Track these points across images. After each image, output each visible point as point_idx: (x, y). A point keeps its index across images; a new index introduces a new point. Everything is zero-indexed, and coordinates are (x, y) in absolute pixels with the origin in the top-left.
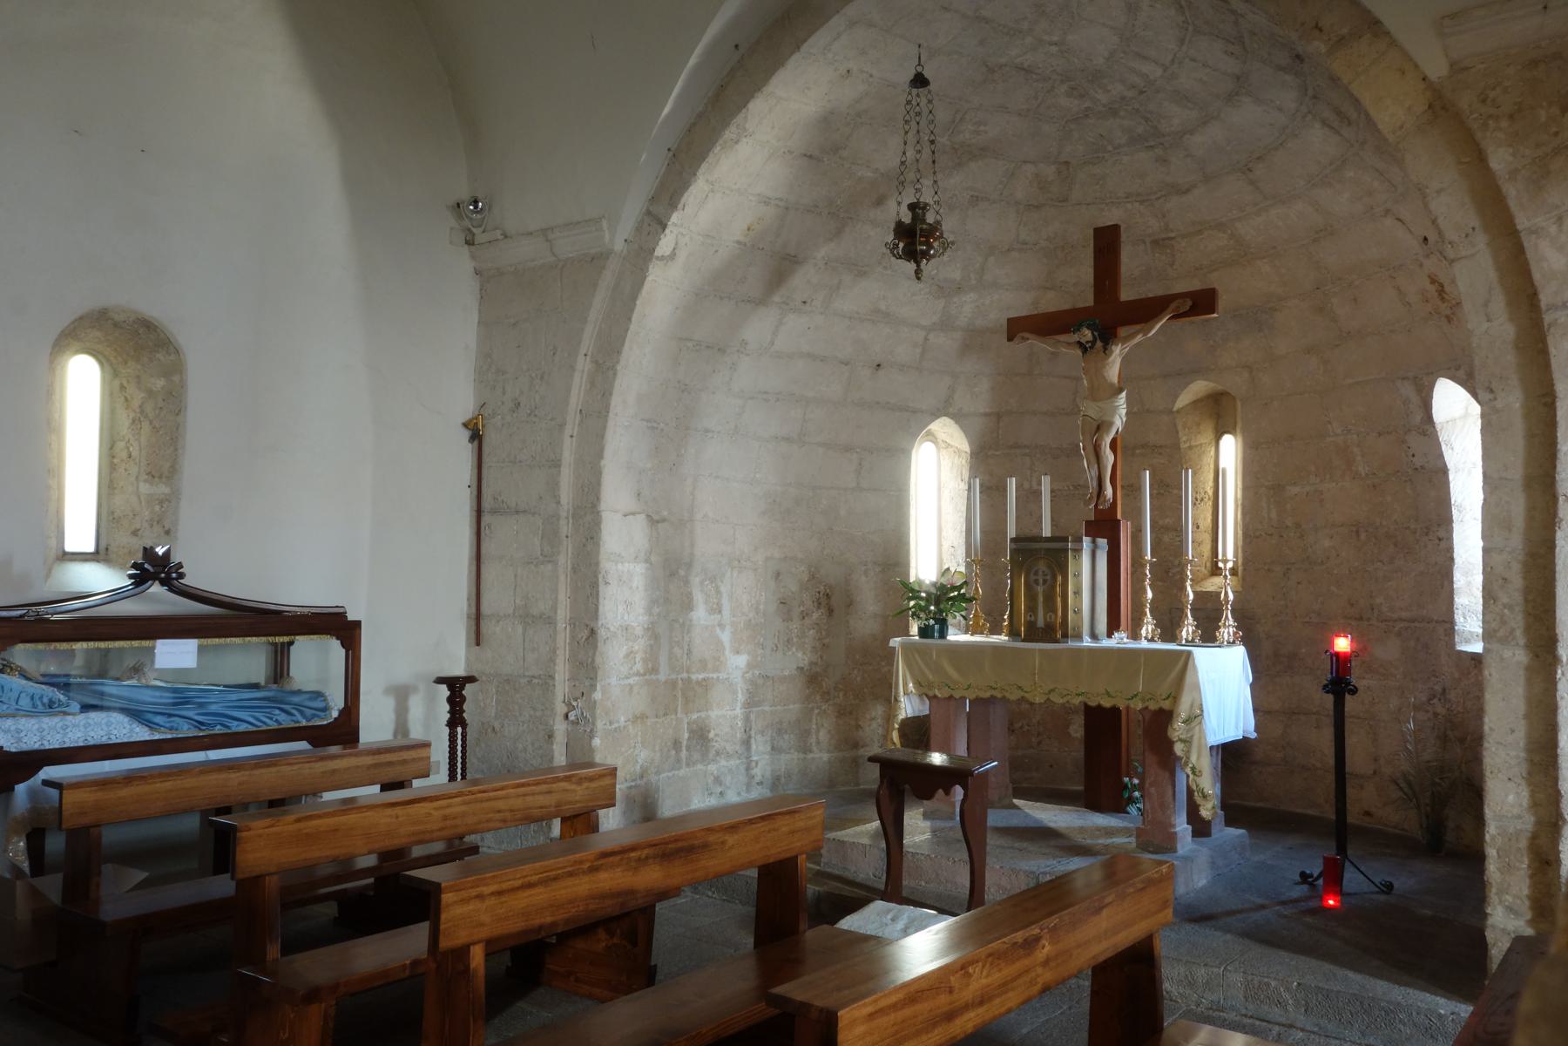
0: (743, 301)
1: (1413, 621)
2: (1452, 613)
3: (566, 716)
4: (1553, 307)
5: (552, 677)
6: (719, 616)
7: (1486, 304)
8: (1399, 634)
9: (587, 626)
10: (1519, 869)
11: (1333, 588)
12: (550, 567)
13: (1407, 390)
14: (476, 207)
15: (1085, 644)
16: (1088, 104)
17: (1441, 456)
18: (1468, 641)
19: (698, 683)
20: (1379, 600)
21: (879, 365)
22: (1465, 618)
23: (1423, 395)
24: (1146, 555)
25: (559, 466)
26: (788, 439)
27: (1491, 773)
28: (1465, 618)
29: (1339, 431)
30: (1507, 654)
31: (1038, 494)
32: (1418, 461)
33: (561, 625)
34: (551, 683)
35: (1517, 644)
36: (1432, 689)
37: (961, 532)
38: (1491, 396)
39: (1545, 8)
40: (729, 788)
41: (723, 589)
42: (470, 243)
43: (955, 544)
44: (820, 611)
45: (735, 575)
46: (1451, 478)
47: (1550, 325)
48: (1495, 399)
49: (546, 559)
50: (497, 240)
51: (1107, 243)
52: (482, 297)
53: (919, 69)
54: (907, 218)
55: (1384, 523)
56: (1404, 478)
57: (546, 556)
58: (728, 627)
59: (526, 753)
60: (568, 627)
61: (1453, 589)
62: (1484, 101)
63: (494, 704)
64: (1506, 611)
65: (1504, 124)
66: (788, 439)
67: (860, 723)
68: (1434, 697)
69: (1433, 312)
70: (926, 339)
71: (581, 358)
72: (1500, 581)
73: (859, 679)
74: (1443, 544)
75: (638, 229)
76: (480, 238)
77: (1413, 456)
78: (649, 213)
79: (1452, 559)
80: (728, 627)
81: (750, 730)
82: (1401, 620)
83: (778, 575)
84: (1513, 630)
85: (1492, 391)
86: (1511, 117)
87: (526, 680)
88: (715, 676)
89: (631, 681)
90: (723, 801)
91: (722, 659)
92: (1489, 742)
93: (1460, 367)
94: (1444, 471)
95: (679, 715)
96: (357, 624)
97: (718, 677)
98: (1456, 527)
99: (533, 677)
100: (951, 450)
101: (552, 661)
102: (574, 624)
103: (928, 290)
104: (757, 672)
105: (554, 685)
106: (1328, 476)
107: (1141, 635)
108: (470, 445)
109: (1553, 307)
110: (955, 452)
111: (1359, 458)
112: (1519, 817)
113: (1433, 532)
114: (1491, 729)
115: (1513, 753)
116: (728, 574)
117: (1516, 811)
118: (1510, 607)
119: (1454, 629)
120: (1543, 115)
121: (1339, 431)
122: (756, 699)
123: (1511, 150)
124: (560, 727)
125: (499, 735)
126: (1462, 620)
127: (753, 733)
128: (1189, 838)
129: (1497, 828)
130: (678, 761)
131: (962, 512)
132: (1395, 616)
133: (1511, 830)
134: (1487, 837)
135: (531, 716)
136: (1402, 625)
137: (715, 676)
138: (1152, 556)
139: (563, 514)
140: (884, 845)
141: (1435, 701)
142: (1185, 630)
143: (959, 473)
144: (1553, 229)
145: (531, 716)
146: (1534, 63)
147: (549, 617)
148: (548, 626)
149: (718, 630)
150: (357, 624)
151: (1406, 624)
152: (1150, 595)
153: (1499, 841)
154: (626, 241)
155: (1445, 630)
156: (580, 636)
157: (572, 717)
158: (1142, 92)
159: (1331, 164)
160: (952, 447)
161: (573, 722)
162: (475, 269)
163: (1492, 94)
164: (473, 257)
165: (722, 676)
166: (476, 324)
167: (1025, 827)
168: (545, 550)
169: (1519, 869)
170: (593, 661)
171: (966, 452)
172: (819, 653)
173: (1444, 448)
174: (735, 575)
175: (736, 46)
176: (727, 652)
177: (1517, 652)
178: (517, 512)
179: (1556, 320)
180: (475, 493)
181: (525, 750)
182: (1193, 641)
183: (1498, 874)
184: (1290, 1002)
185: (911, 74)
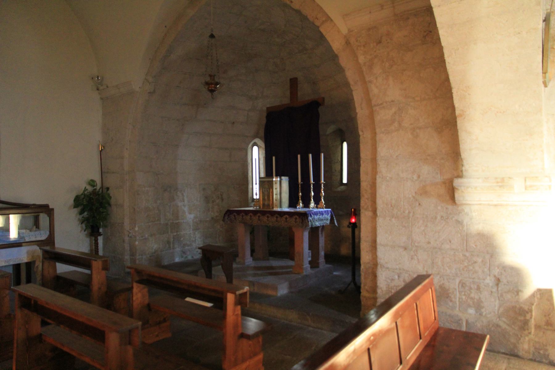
3: (129, 236)
4: (375, 106)
6: (183, 203)
14: (98, 79)
15: (298, 210)
16: (284, 40)
19: (176, 223)
24: (322, 181)
35: (369, 210)
42: (98, 89)
51: (294, 82)
53: (212, 32)
54: (208, 79)
65: (362, 48)
76: (101, 88)
78: (146, 79)
83: (204, 189)
84: (368, 206)
86: (364, 46)
88: (182, 221)
89: (150, 224)
90: (186, 259)
95: (169, 233)
96: (53, 209)
107: (310, 207)
109: (375, 106)
112: (369, 263)
118: (368, 199)
120: (372, 45)
124: (127, 239)
127: (197, 238)
128: (309, 269)
130: (170, 247)
134: (361, 269)
137: (182, 221)
138: (324, 181)
142: (311, 204)
144: (375, 81)
146: (369, 29)
149: (183, 207)
150: (53, 209)
152: (313, 194)
154: (139, 88)
164: (100, 94)
167: (84, 273)
175: (166, 26)
176: (187, 213)
177: (27, 231)
179: (376, 110)
182: (314, 208)
185: (209, 34)
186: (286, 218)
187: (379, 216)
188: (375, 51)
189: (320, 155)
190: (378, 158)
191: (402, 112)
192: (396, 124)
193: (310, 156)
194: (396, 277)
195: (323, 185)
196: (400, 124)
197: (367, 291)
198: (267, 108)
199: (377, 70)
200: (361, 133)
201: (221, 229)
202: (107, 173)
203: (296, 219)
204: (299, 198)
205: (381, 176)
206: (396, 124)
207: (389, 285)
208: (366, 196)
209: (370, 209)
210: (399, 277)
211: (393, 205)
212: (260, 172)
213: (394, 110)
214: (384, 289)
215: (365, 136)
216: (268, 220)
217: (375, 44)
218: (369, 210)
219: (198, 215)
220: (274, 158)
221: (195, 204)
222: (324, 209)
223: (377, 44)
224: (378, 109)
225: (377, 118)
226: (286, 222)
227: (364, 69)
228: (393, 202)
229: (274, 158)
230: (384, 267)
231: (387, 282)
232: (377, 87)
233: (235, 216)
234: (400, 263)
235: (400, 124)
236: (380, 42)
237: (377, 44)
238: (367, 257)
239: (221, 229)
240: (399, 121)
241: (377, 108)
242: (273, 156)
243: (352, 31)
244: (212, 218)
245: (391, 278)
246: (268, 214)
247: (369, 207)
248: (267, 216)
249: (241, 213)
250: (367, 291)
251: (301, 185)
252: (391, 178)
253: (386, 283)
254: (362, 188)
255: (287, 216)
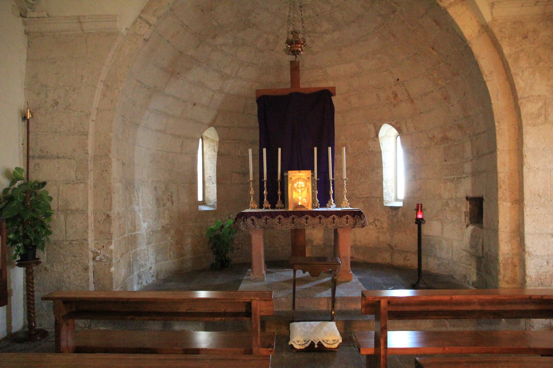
0: (161, 68)
1: (367, 198)
2: (383, 195)
4: (521, 98)
5: (86, 240)
6: (139, 206)
7: (497, 96)
8: (363, 202)
9: (105, 213)
10: (508, 269)
11: (339, 189)
12: (82, 185)
13: (371, 127)
17: (380, 147)
18: (386, 203)
20: (356, 192)
21: (195, 104)
22: (386, 196)
23: (377, 128)
25: (87, 135)
26: (160, 131)
27: (501, 241)
28: (386, 196)
29: (344, 139)
30: (505, 204)
31: (246, 158)
32: (370, 149)
33: (90, 214)
34: (85, 242)
35: (507, 201)
36: (375, 218)
37: (214, 171)
38: (499, 124)
39: (522, 5)
40: (143, 280)
41: (139, 195)
43: (211, 175)
44: (169, 203)
45: (143, 188)
46: (382, 154)
47: (520, 104)
48: (500, 125)
49: (80, 181)
50: (44, 17)
52: (29, 46)
54: (291, 37)
55: (357, 168)
56: (365, 154)
57: (79, 180)
58: (141, 211)
59: (70, 279)
60: (93, 215)
61: (383, 188)
62: (501, 32)
63: (45, 256)
64: (504, 191)
65: (507, 40)
66: (160, 131)
67: (184, 247)
68: (376, 220)
69: (388, 103)
70: (213, 96)
71: (99, 82)
72: (503, 182)
73: (182, 229)
74: (379, 174)
75: (134, 24)
76: (30, 14)
77: (369, 147)
78: (140, 17)
79: (382, 179)
80: (141, 211)
81: (149, 254)
82: (363, 197)
84: (506, 197)
85: (499, 123)
87: (68, 243)
91: (140, 225)
92: (500, 232)
93: (393, 121)
94: (380, 152)
97: (139, 233)
98: (384, 169)
99: (73, 240)
100: (209, 140)
101: (86, 231)
102: (96, 213)
103: (218, 76)
104: (150, 229)
105: (88, 244)
106: (338, 153)
108: (23, 123)
109: (521, 98)
110: (211, 141)
111: (349, 148)
112: (508, 253)
113: (375, 171)
114: (500, 227)
115: (506, 234)
116: (141, 189)
117: (507, 252)
118: (506, 190)
119: (383, 200)
121: (344, 139)
122: (150, 241)
123: (509, 48)
125: (50, 271)
126: (385, 197)
129: (502, 258)
131: (215, 163)
132: (361, 196)
133: (506, 258)
135: (72, 260)
136: (363, 199)
139: (89, 159)
140: (473, 296)
141: (376, 221)
143: (213, 148)
144: (521, 74)
145: (72, 260)
146: (515, 23)
147: (82, 210)
148: (82, 215)
151: (365, 199)
153: (503, 262)
154: (126, 28)
155: (380, 200)
156: (100, 219)
157: (98, 258)
158: (318, 15)
159: (372, 52)
160: (210, 139)
161: (97, 261)
162: (25, 31)
163: (504, 30)
164: (25, 24)
165: (140, 232)
166: (26, 60)
168: (79, 177)
169: (508, 269)
170: (110, 230)
171: (217, 141)
172: (170, 220)
173: (381, 145)
174: (143, 188)
177: (507, 203)
178: (58, 158)
179: (522, 102)
180: (26, 148)
181: (69, 277)
183: (503, 271)
184: (448, 324)
186: (334, 219)
187: (527, 205)
188: (521, 45)
189: (342, 151)
190: (525, 149)
191: (549, 107)
192: (542, 118)
193: (280, 149)
194: (545, 263)
195: (345, 182)
196: (546, 119)
197: (507, 282)
198: (257, 91)
199: (523, 63)
200: (497, 124)
201: (171, 241)
202: (40, 157)
203: (347, 218)
204: (330, 196)
205: (528, 167)
206: (542, 118)
207: (538, 272)
208: (504, 187)
209: (509, 200)
210: (547, 262)
211: (540, 195)
212: (205, 168)
213: (540, 104)
214: (534, 277)
215: (501, 127)
216: (307, 223)
217: (521, 38)
218: (507, 201)
219: (151, 224)
220: (316, 149)
221: (149, 209)
222: (318, 209)
223: (523, 39)
224: (524, 102)
225: (524, 111)
226: (293, 223)
227: (510, 61)
228: (541, 191)
229: (316, 149)
230: (532, 255)
231: (536, 269)
232: (523, 81)
233: (253, 220)
234: (548, 250)
235: (546, 119)
236: (526, 37)
237: (523, 39)
238: (506, 248)
239: (171, 241)
240: (545, 116)
241: (524, 101)
242: (279, 147)
243: (496, 20)
244: (163, 227)
245: (540, 265)
246: (252, 217)
247: (508, 197)
248: (278, 218)
249: (277, 216)
250: (507, 282)
251: (317, 181)
252: (538, 169)
253: (535, 271)
254: (499, 179)
255: (335, 216)
